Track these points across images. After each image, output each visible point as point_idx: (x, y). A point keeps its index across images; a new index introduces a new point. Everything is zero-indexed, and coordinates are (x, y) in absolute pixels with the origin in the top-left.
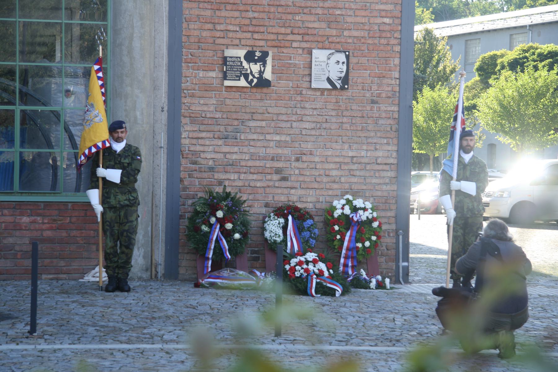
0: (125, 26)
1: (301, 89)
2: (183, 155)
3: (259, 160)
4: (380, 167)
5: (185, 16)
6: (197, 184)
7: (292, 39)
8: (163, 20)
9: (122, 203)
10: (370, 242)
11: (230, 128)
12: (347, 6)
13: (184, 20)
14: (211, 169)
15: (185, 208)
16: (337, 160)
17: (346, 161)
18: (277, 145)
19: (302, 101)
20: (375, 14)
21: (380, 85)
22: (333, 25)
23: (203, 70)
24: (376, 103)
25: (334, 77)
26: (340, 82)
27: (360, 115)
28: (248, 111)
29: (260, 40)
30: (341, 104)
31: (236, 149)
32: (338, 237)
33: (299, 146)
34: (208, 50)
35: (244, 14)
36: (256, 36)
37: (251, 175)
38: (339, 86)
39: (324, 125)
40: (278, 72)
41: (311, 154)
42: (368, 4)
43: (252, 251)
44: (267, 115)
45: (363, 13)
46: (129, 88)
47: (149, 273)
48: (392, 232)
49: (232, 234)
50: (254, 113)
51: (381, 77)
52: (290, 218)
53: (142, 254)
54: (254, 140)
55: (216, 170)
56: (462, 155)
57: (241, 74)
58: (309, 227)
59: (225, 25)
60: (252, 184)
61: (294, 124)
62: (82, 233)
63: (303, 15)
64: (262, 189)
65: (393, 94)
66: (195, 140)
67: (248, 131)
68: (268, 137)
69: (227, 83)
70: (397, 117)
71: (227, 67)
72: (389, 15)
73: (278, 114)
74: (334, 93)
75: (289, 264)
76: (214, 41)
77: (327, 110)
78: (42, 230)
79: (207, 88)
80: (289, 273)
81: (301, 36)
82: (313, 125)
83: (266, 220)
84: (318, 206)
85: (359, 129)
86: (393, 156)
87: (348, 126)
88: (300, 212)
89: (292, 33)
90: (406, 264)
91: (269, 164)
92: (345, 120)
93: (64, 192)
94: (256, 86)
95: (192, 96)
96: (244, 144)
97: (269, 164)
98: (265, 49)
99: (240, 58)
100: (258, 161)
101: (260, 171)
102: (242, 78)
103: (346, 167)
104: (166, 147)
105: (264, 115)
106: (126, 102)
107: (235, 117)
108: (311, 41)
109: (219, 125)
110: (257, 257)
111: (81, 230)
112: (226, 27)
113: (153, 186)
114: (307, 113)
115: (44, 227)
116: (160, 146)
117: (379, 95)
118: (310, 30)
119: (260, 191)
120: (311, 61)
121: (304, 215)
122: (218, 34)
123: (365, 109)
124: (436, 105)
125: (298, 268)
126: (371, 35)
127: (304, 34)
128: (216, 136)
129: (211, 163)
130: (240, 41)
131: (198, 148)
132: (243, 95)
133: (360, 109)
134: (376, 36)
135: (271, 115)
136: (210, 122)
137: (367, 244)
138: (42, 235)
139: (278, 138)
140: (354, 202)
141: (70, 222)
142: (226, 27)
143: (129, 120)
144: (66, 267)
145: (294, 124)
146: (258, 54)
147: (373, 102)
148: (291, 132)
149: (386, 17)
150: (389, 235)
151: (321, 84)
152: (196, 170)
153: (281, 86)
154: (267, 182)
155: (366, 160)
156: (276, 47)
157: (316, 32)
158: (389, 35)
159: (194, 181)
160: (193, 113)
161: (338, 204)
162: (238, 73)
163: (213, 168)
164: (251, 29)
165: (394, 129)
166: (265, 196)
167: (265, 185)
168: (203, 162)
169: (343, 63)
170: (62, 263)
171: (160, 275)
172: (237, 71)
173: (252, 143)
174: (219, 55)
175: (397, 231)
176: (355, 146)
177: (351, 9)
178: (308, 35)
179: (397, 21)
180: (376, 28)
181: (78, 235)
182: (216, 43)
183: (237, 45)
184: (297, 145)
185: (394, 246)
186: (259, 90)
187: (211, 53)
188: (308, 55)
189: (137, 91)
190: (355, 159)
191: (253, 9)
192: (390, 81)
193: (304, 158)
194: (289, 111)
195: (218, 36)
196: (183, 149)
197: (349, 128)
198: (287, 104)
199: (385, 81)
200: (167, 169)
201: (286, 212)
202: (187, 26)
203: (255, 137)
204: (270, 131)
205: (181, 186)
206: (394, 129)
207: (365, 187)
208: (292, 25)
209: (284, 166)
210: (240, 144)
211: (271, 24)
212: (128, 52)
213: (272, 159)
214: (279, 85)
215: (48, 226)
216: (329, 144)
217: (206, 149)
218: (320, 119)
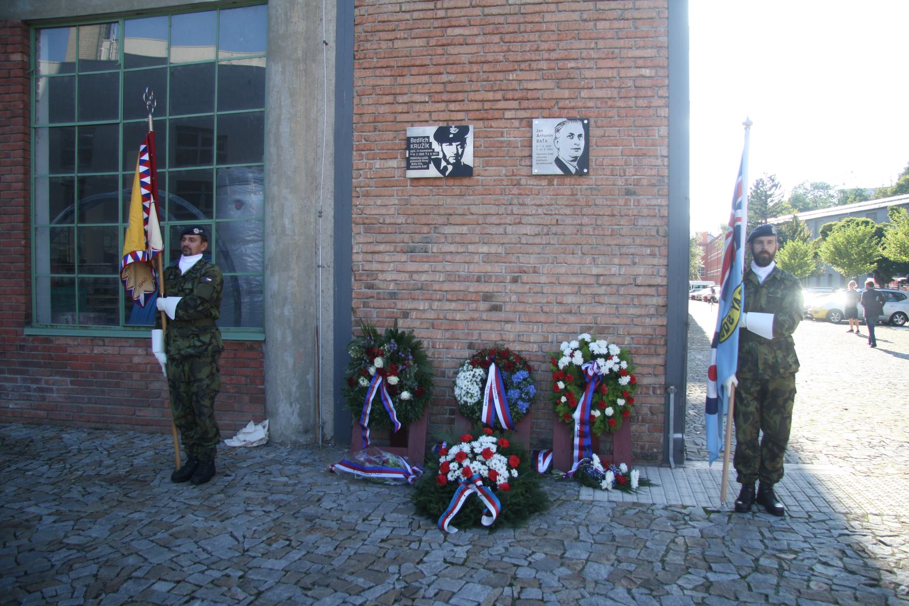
4: (641, 290)
9: (183, 352)
10: (614, 409)
11: (417, 237)
14: (393, 296)
17: (588, 282)
18: (485, 259)
19: (520, 194)
20: (628, 63)
21: (638, 167)
22: (565, 83)
24: (634, 193)
25: (566, 157)
26: (575, 164)
27: (609, 213)
28: (442, 211)
31: (426, 267)
32: (564, 399)
35: (435, 78)
36: (452, 106)
37: (448, 303)
38: (573, 171)
39: (554, 229)
40: (484, 155)
41: (535, 272)
42: (617, 51)
43: (451, 410)
44: (470, 217)
45: (610, 63)
48: (660, 388)
50: (451, 215)
52: (492, 368)
53: (297, 411)
55: (400, 296)
56: (754, 270)
58: (520, 383)
60: (449, 316)
63: (519, 72)
64: (464, 323)
65: (659, 181)
66: (370, 255)
68: (471, 248)
69: (412, 174)
70: (666, 214)
72: (649, 64)
74: (567, 180)
79: (386, 182)
82: (537, 230)
85: (606, 233)
86: (662, 274)
88: (507, 359)
90: (679, 436)
91: (473, 287)
92: (585, 220)
94: (453, 175)
95: (367, 195)
96: (437, 259)
97: (473, 287)
98: (464, 124)
99: (428, 137)
100: (458, 283)
102: (432, 166)
103: (588, 291)
106: (272, 207)
107: (424, 221)
108: (533, 109)
114: (528, 211)
117: (637, 183)
119: (460, 325)
121: (515, 363)
122: (400, 108)
123: (616, 203)
124: (795, 249)
127: (523, 99)
129: (392, 286)
130: (430, 115)
131: (375, 266)
132: (435, 190)
133: (608, 203)
134: (630, 95)
135: (475, 217)
136: (390, 230)
137: (609, 411)
139: (485, 249)
145: (510, 229)
146: (453, 130)
147: (628, 193)
148: (505, 241)
149: (645, 67)
150: (654, 393)
151: (544, 166)
153: (487, 175)
154: (471, 313)
155: (619, 280)
158: (650, 93)
161: (566, 347)
163: (395, 293)
164: (445, 97)
165: (661, 232)
166: (468, 334)
167: (468, 318)
168: (381, 285)
169: (580, 136)
173: (448, 257)
175: (666, 387)
176: (601, 259)
185: (662, 408)
186: (457, 182)
187: (391, 135)
190: (602, 278)
191: (449, 70)
192: (653, 161)
193: (525, 278)
194: (502, 210)
197: (591, 233)
198: (498, 200)
199: (646, 161)
203: (452, 248)
204: (473, 241)
206: (661, 232)
207: (617, 321)
208: (503, 88)
209: (495, 290)
211: (473, 88)
213: (478, 280)
214: (487, 173)
216: (561, 257)
217: (385, 267)
218: (547, 220)
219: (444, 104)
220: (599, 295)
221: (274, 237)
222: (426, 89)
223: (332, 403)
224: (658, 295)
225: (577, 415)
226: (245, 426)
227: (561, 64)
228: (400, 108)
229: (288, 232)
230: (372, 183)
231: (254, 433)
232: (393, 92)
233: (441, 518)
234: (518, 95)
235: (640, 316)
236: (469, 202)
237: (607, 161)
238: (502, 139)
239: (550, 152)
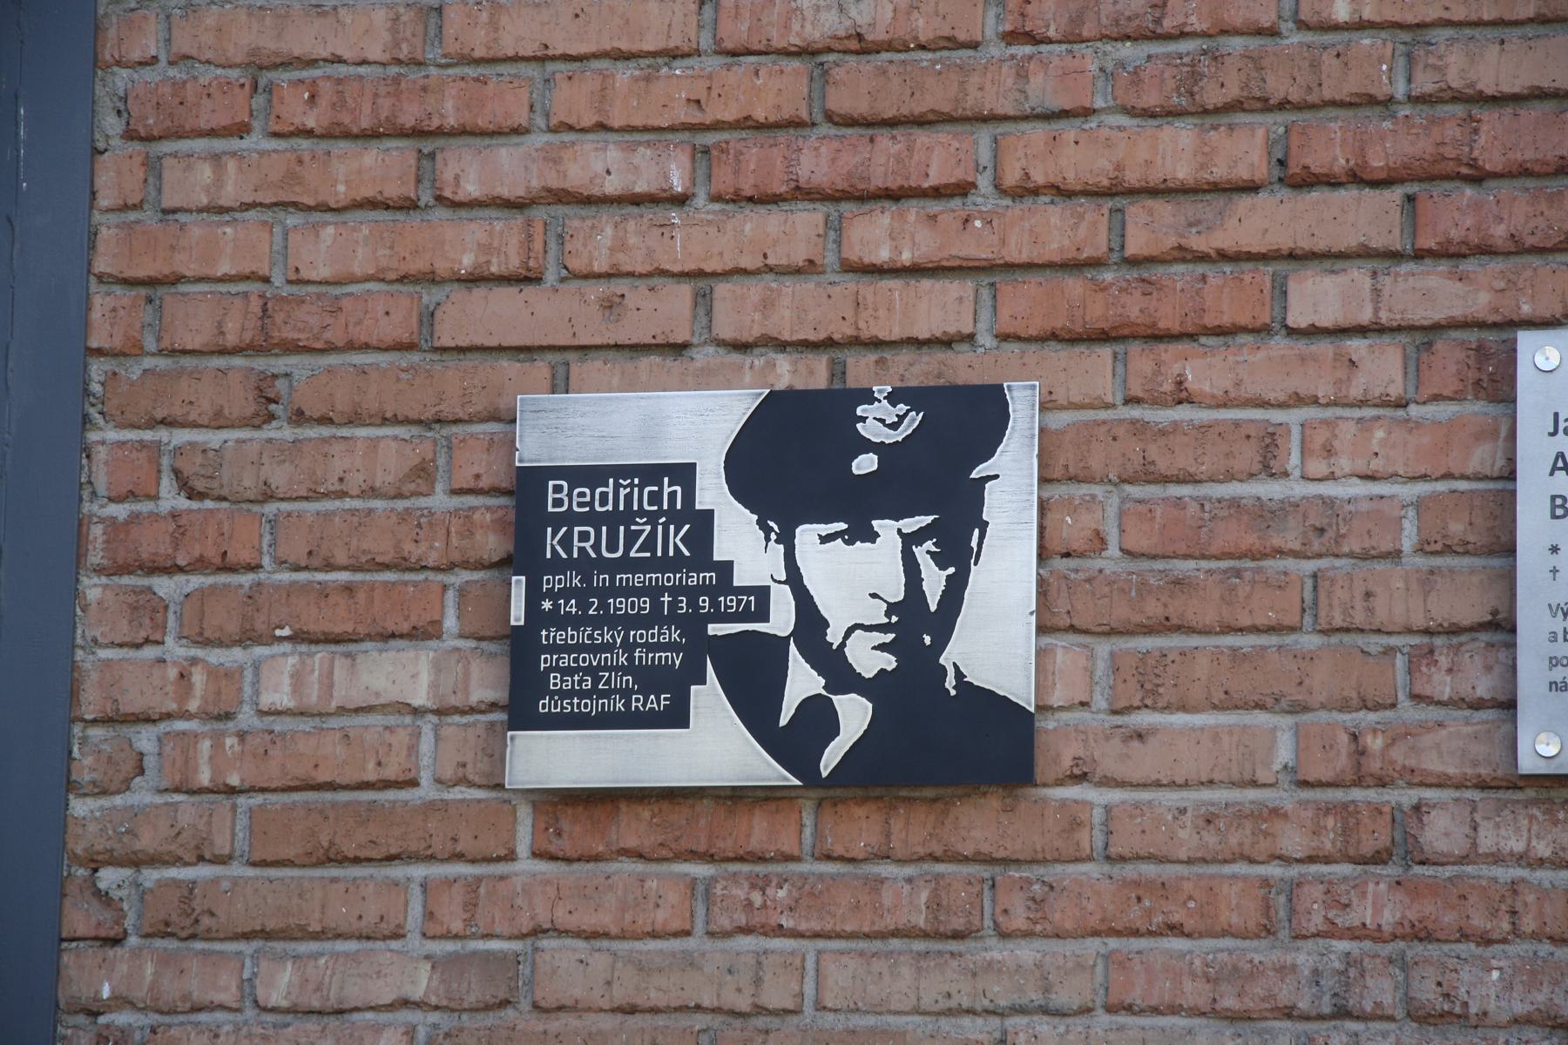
1: (1406, 797)
7: (1283, 240)
13: (111, 124)
19: (1421, 934)
36: (876, 235)
40: (1121, 613)
57: (698, 648)
59: (539, 140)
71: (595, 601)
76: (429, 317)
79: (340, 822)
81: (1396, 194)
95: (184, 923)
98: (963, 369)
99: (684, 474)
102: (709, 698)
108: (1518, 248)
112: (552, 158)
122: (463, 244)
127: (1432, 173)
130: (703, 301)
132: (736, 889)
142: (552, 158)
146: (880, 422)
162: (661, 644)
164: (818, 160)
172: (655, 618)
178: (1478, 177)
186: (912, 828)
188: (1475, 408)
195: (467, 262)
198: (1240, 975)
208: (1278, 86)
211: (1043, 90)
219: (807, 220)
222: (672, 97)
230: (230, 827)
232: (408, 120)
234: (1391, 144)
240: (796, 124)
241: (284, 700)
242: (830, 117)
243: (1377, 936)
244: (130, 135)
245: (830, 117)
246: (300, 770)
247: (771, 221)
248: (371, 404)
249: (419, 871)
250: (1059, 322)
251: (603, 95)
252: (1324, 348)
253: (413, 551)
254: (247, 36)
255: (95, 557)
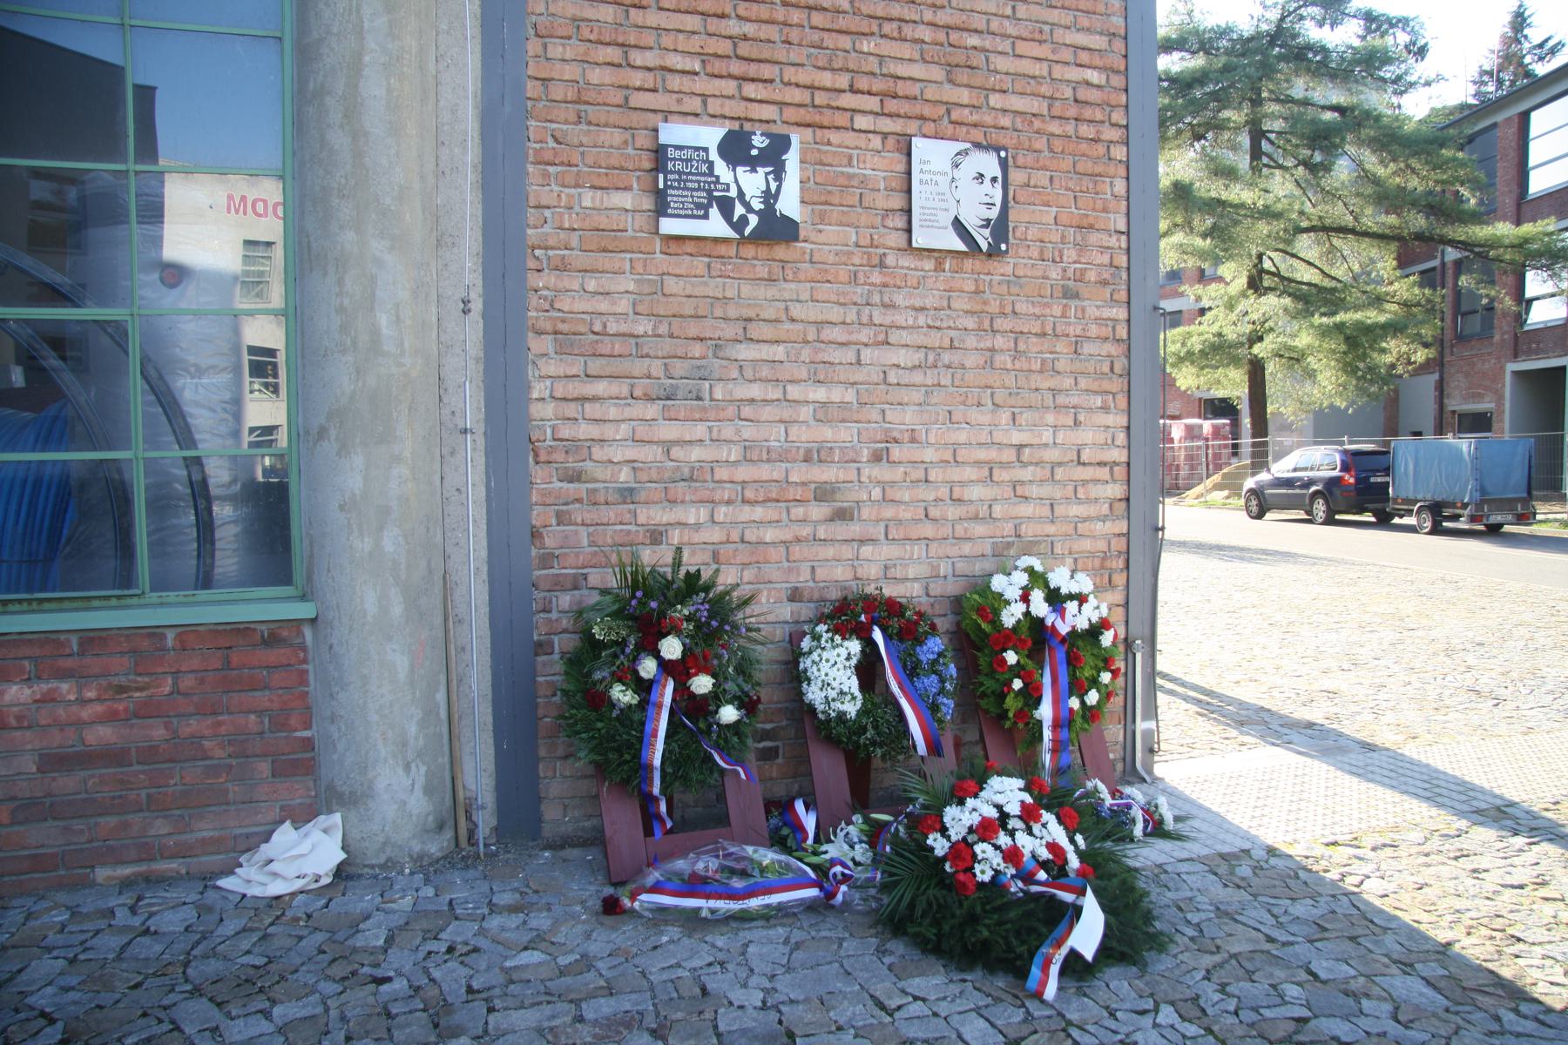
0: (335, 30)
2: (536, 455)
3: (768, 461)
4: (1088, 473)
5: (534, 18)
6: (585, 542)
8: (464, 25)
11: (679, 368)
12: (994, 26)
13: (532, 32)
14: (627, 495)
15: (550, 620)
16: (982, 454)
18: (820, 415)
20: (1067, 55)
21: (1081, 248)
22: (962, 76)
23: (593, 187)
24: (1077, 296)
26: (987, 232)
28: (732, 312)
29: (761, 101)
30: (987, 295)
31: (700, 430)
32: (1017, 684)
33: (880, 418)
34: (606, 125)
35: (714, 25)
36: (750, 90)
37: (747, 508)
38: (984, 246)
39: (946, 357)
40: (815, 199)
41: (913, 440)
42: (1047, 28)
44: (788, 326)
45: (1038, 51)
46: (350, 235)
47: (449, 834)
49: (712, 708)
51: (1085, 227)
52: (877, 635)
53: (421, 781)
54: (753, 400)
55: (642, 496)
58: (935, 662)
61: (867, 354)
62: (219, 724)
66: (573, 405)
67: (735, 374)
68: (794, 392)
69: (669, 226)
73: (820, 324)
74: (968, 264)
75: (943, 830)
76: (627, 99)
77: (954, 314)
78: (80, 724)
79: (606, 240)
80: (948, 867)
82: (918, 357)
83: (806, 644)
84: (936, 589)
87: (1009, 360)
88: (903, 615)
89: (854, 90)
92: (999, 342)
93: (153, 589)
94: (758, 237)
95: (562, 267)
96: (722, 415)
99: (706, 150)
101: (774, 496)
102: (714, 212)
104: (480, 429)
105: (779, 326)
106: (340, 282)
107: (693, 331)
109: (647, 356)
110: (770, 749)
111: (214, 713)
113: (446, 557)
114: (900, 319)
115: (86, 713)
116: (461, 425)
117: (1080, 278)
118: (900, 83)
120: (909, 173)
122: (637, 79)
123: (1048, 311)
125: (982, 849)
126: (1055, 112)
128: (637, 393)
129: (625, 475)
130: (705, 103)
131: (585, 431)
132: (717, 265)
133: (1037, 311)
135: (800, 326)
136: (617, 349)
138: (82, 740)
139: (820, 394)
140: (1050, 576)
141: (176, 691)
143: (354, 343)
144: (176, 837)
145: (867, 354)
146: (759, 141)
147: (1070, 294)
148: (859, 377)
151: (934, 234)
152: (580, 501)
153: (827, 240)
155: (1052, 455)
156: (809, 125)
157: (915, 89)
158: (1099, 117)
159: (576, 532)
160: (563, 321)
161: (1008, 585)
163: (631, 490)
164: (736, 67)
166: (790, 570)
168: (600, 472)
169: (994, 180)
170: (161, 827)
171: (483, 831)
173: (747, 411)
174: (643, 140)
176: (1025, 417)
177: (1005, 36)
179: (1118, 81)
180: (1068, 93)
181: (206, 733)
182: (632, 105)
183: (697, 115)
184: (875, 415)
186: (763, 252)
187: (617, 137)
189: (377, 246)
193: (896, 452)
195: (638, 84)
196: (535, 436)
197: (1009, 366)
198: (845, 294)
199: (1094, 238)
200: (488, 499)
201: (863, 618)
202: (540, 51)
203: (755, 391)
204: (797, 376)
205: (534, 552)
206: (1117, 369)
207: (1051, 529)
208: (851, 66)
209: (841, 477)
210: (712, 415)
211: (793, 58)
212: (345, 116)
214: (821, 238)
215: (99, 708)
217: (608, 431)
218: (934, 339)
219: (733, 84)
220: (1022, 483)
221: (350, 358)
222: (695, 44)
223: (492, 751)
224: (1114, 481)
225: (1045, 712)
226: (267, 838)
227: (954, 36)
228: (637, 79)
229: (388, 347)
230: (574, 239)
231: (301, 856)
232: (620, 40)
233: (1035, 971)
234: (878, 85)
235: (1085, 520)
236: (787, 296)
237: (1033, 233)
238: (850, 170)
239: (944, 205)
240: (728, 57)
241: (589, 204)
242: (737, 57)
243: (875, 285)
244: (537, 35)
245: (737, 57)
246: (595, 225)
247: (723, 82)
248: (611, 121)
249: (629, 256)
250: (798, 120)
251: (676, 41)
252: (863, 135)
253: (625, 165)
254: (571, 11)
255: (531, 159)
